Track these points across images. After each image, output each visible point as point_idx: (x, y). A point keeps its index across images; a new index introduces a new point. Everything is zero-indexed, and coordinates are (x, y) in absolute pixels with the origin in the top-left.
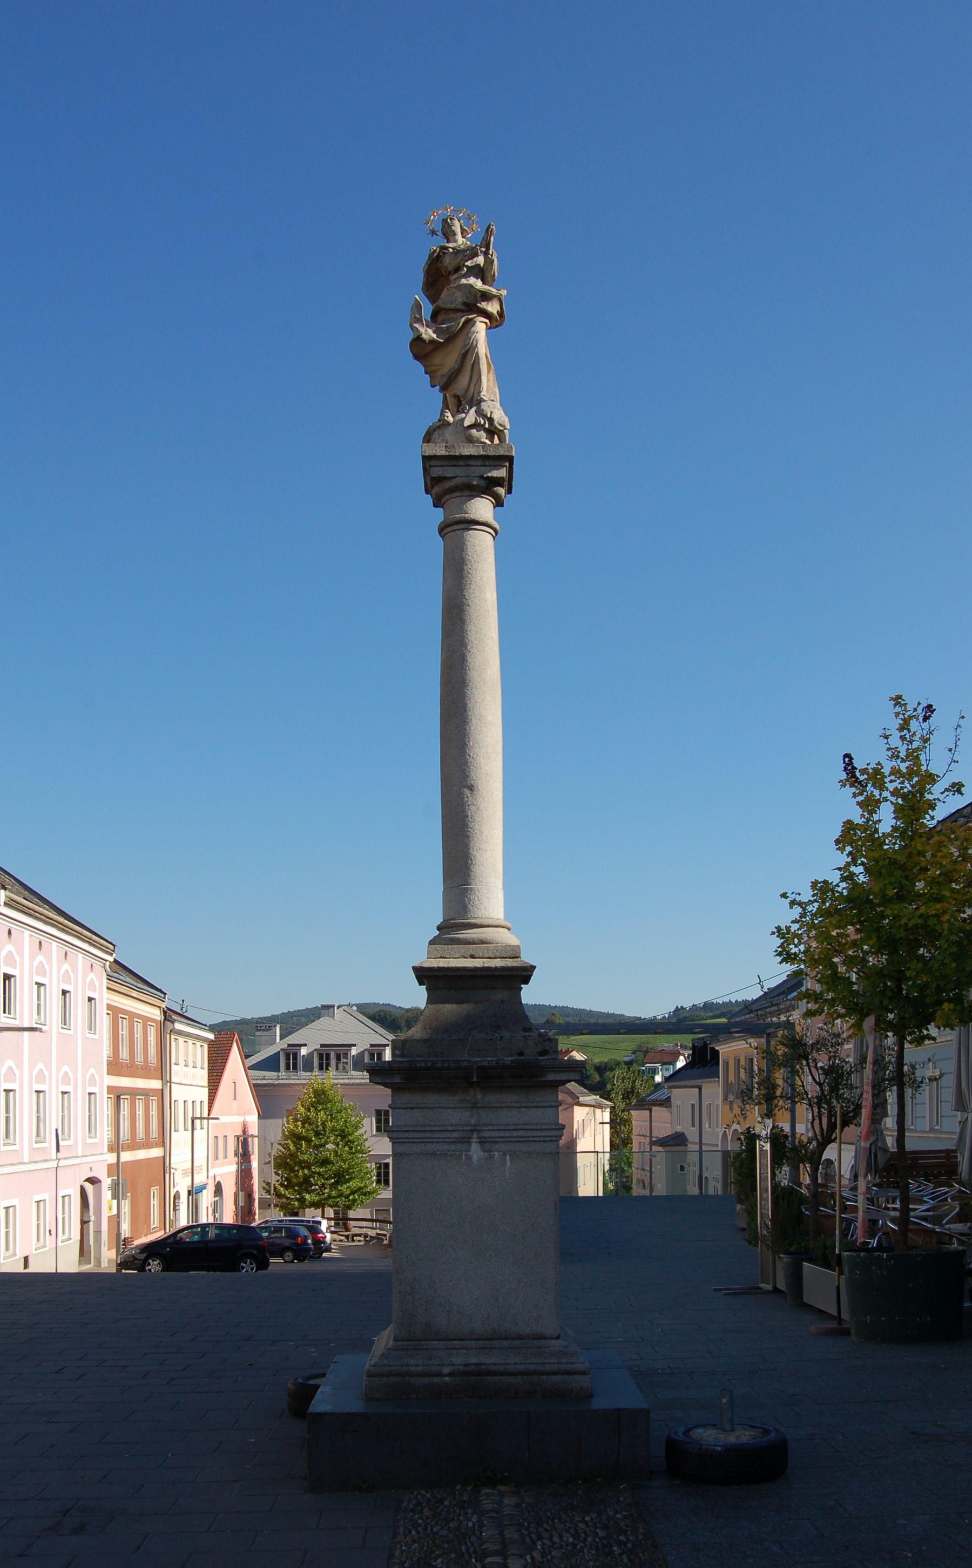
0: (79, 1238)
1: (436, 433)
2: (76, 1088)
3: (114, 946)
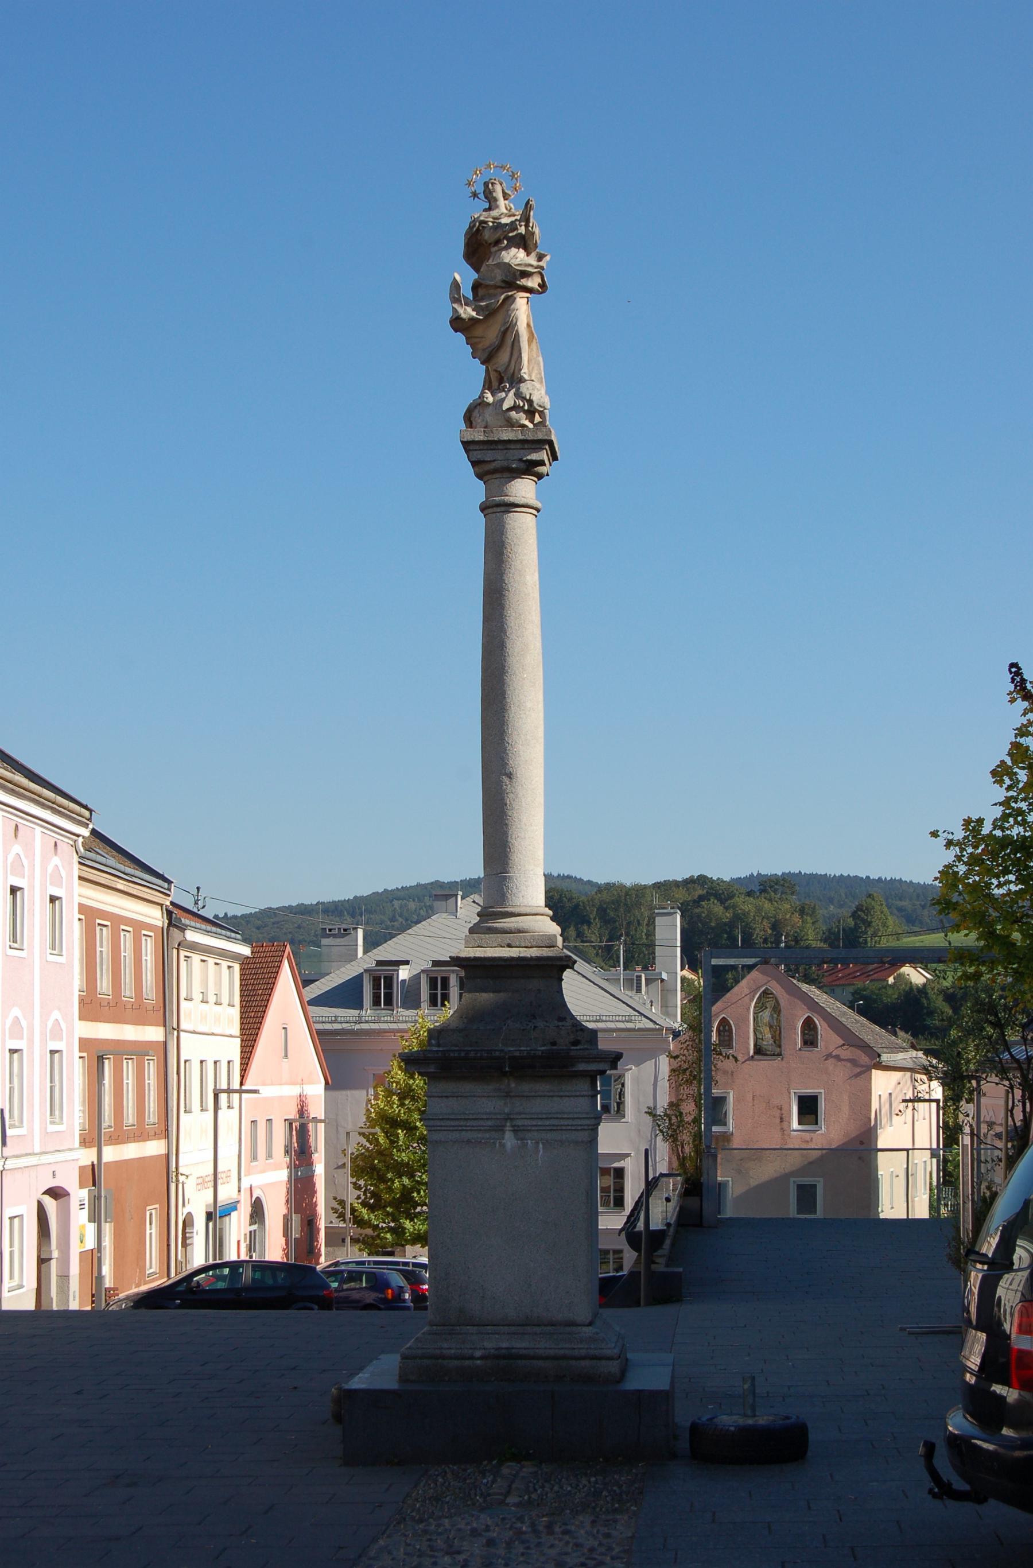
0: (35, 1286)
1: (477, 411)
2: (31, 1041)
3: (91, 811)
